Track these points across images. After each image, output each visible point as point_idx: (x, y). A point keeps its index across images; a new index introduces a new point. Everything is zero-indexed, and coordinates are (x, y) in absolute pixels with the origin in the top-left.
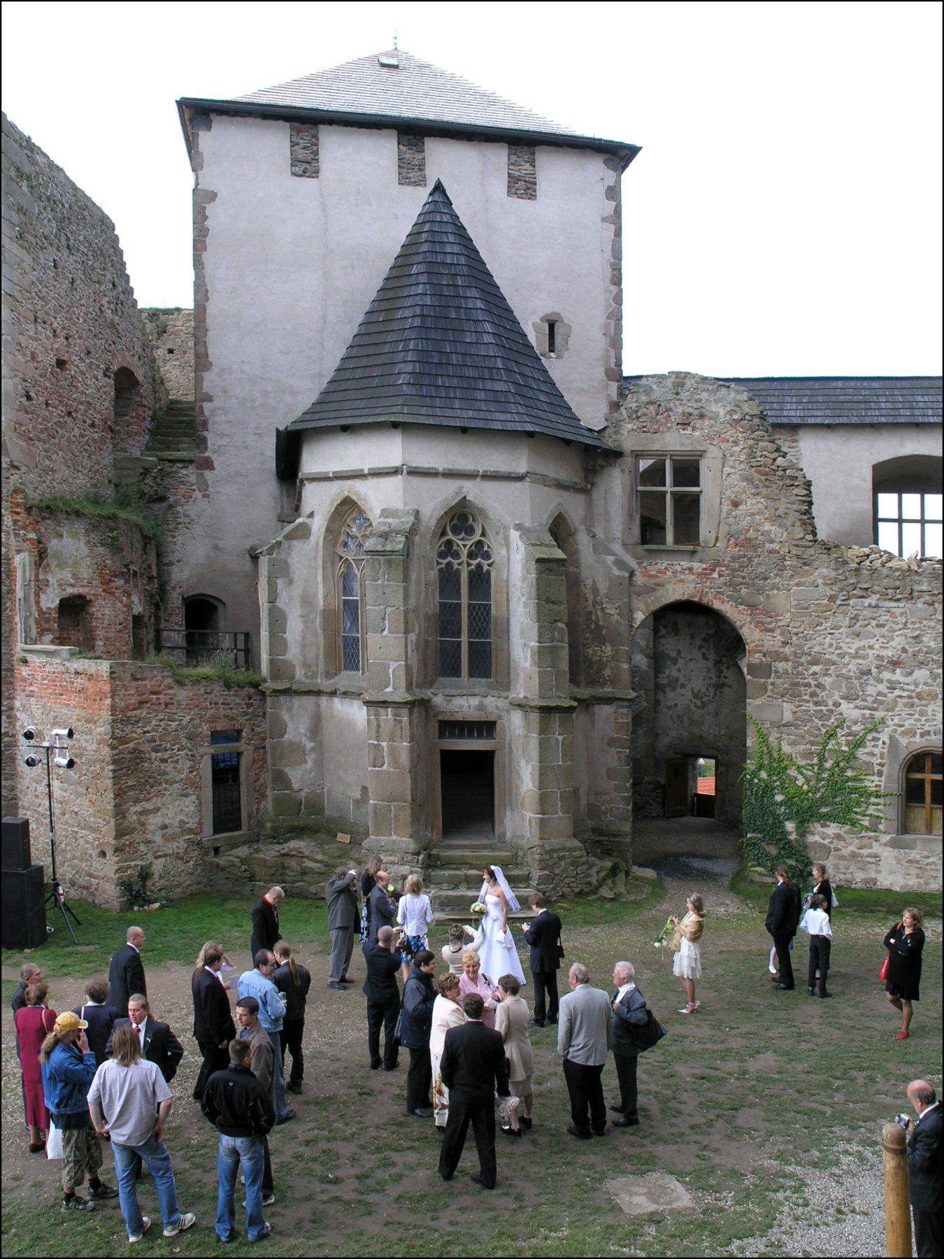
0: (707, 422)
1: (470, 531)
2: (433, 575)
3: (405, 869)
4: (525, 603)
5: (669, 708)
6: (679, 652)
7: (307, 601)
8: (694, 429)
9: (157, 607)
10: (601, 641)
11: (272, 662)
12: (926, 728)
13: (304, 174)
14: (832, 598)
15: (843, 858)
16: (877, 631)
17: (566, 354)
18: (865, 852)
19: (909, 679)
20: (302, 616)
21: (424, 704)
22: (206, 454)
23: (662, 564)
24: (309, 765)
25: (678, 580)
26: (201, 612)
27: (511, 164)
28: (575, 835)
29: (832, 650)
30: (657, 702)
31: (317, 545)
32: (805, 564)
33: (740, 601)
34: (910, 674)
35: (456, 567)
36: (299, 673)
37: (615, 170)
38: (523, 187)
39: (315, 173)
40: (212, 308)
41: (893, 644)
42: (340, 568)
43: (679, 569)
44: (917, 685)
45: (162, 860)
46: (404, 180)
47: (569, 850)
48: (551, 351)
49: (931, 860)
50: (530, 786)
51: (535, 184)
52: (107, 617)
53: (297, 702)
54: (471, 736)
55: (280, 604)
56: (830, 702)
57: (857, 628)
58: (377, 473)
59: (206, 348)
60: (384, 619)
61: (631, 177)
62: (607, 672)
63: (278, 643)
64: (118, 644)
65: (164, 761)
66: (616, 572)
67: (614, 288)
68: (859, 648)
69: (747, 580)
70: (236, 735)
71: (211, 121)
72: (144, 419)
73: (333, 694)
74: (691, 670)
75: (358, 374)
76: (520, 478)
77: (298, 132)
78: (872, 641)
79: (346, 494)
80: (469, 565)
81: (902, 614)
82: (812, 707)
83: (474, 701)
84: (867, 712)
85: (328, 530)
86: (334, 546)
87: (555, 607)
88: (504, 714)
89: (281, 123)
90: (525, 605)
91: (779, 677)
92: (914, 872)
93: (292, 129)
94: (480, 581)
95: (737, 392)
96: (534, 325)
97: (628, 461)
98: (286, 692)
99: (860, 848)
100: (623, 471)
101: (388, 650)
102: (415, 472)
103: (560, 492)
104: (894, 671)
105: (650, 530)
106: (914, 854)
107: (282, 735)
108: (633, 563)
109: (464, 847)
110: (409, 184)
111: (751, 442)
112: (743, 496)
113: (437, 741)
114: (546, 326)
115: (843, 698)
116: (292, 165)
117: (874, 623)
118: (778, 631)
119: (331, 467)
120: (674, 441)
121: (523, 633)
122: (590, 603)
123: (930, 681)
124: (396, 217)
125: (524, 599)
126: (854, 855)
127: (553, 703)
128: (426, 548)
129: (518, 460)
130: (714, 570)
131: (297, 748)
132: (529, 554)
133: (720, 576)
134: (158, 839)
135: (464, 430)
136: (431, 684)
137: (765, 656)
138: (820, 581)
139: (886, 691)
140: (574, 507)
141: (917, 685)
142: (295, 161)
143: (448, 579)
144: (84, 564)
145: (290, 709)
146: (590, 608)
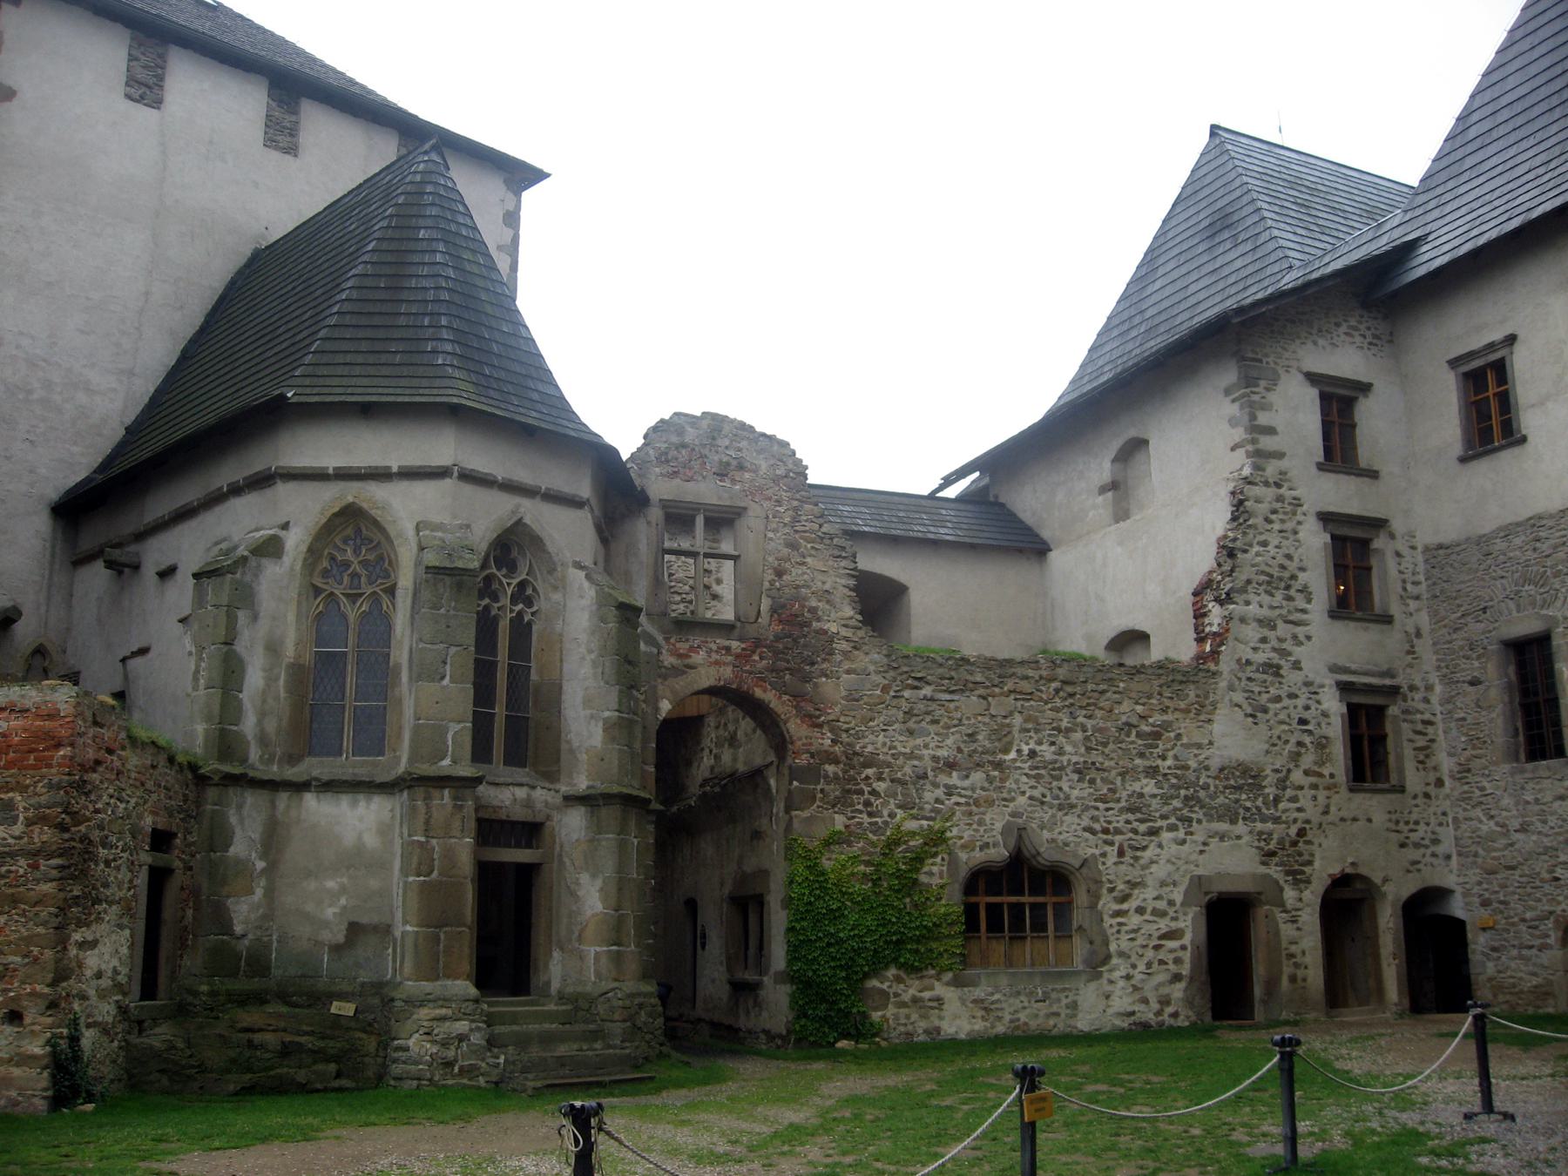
0: (747, 475)
1: (512, 568)
3: (462, 1026)
4: (593, 662)
7: (273, 648)
8: (733, 481)
12: (986, 839)
13: (140, 100)
14: (885, 689)
15: (903, 1005)
16: (932, 728)
18: (927, 995)
19: (966, 783)
20: (265, 670)
24: (259, 892)
29: (885, 750)
31: (292, 569)
32: (855, 648)
33: (782, 689)
34: (967, 777)
36: (254, 754)
39: (157, 103)
41: (949, 742)
42: (318, 604)
43: (714, 647)
44: (973, 790)
49: (996, 997)
50: (599, 907)
55: (239, 647)
56: (885, 813)
57: (911, 724)
60: (445, 663)
69: (792, 665)
77: (140, 45)
78: (928, 739)
79: (350, 499)
81: (957, 708)
82: (866, 819)
83: (521, 793)
84: (925, 823)
86: (311, 575)
88: (556, 816)
89: (119, 27)
90: (594, 664)
91: (828, 783)
92: (980, 1013)
100: (649, 523)
102: (468, 477)
104: (950, 775)
106: (978, 993)
109: (512, 1004)
110: (277, 148)
112: (787, 565)
115: (899, 807)
116: (127, 84)
117: (928, 718)
121: (587, 702)
123: (986, 785)
124: (256, 185)
126: (915, 1000)
131: (243, 867)
137: (812, 756)
138: (872, 668)
139: (944, 797)
141: (973, 790)
142: (131, 81)
145: (240, 807)
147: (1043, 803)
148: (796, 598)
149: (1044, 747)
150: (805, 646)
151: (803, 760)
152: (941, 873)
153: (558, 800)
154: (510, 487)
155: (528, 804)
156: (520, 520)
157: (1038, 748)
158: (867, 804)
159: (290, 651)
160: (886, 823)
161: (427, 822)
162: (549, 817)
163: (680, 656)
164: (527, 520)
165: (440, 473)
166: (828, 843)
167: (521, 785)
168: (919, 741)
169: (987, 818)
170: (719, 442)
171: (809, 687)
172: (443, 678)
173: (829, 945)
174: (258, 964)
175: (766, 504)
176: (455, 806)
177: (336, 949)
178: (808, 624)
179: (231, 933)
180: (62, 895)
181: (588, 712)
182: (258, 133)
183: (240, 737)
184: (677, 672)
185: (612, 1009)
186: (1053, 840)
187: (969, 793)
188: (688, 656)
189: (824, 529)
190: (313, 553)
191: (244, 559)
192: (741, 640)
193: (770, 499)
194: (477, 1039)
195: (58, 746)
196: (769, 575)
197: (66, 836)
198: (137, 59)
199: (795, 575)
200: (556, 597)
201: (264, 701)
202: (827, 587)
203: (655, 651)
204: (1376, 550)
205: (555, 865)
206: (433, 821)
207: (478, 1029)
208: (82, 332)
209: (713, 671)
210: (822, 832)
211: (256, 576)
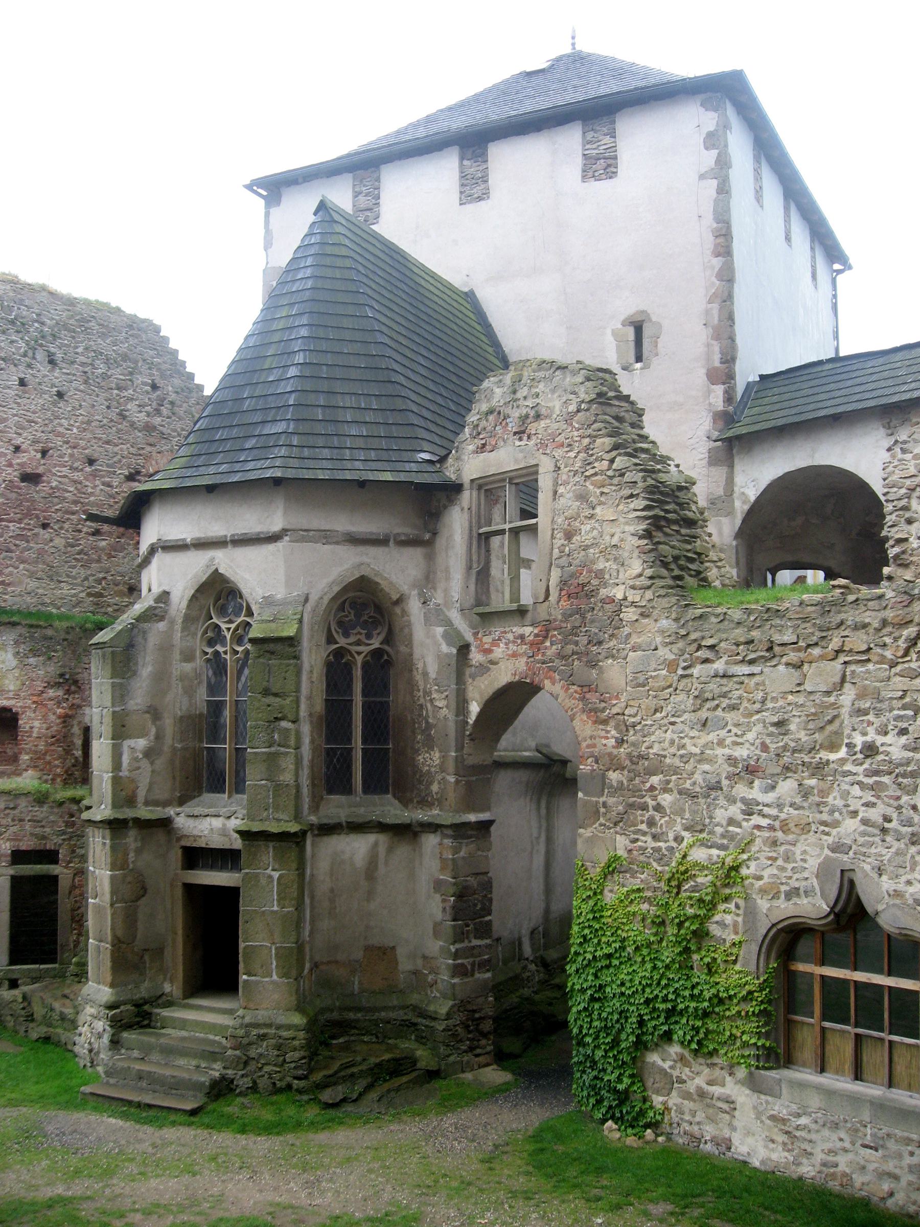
0: (543, 423)
17: (655, 362)
18: (716, 1090)
19: (770, 797)
23: (497, 631)
27: (585, 142)
29: (673, 750)
34: (773, 788)
41: (750, 736)
43: (510, 636)
44: (780, 806)
47: (279, 1027)
48: (639, 359)
51: (615, 158)
52: (35, 730)
56: (671, 836)
64: (48, 758)
67: (717, 262)
68: (705, 746)
76: (273, 538)
78: (723, 733)
82: (651, 844)
83: (217, 823)
87: (278, 700)
93: (354, 179)
96: (615, 333)
99: (710, 1083)
103: (361, 549)
106: (780, 1108)
108: (469, 636)
111: (586, 441)
113: (179, 871)
114: (631, 331)
115: (686, 829)
118: (612, 723)
123: (798, 800)
127: (256, 827)
129: (271, 516)
133: (552, 645)
135: (211, 489)
136: (182, 802)
139: (740, 817)
141: (780, 806)
144: (10, 676)
146: (422, 701)
147: (884, 831)
149: (888, 739)
152: (735, 924)
154: (201, 545)
156: (217, 570)
157: (880, 740)
158: (651, 823)
160: (671, 849)
168: (713, 737)
169: (798, 850)
175: (558, 453)
186: (898, 894)
187: (773, 812)
202: (615, 541)
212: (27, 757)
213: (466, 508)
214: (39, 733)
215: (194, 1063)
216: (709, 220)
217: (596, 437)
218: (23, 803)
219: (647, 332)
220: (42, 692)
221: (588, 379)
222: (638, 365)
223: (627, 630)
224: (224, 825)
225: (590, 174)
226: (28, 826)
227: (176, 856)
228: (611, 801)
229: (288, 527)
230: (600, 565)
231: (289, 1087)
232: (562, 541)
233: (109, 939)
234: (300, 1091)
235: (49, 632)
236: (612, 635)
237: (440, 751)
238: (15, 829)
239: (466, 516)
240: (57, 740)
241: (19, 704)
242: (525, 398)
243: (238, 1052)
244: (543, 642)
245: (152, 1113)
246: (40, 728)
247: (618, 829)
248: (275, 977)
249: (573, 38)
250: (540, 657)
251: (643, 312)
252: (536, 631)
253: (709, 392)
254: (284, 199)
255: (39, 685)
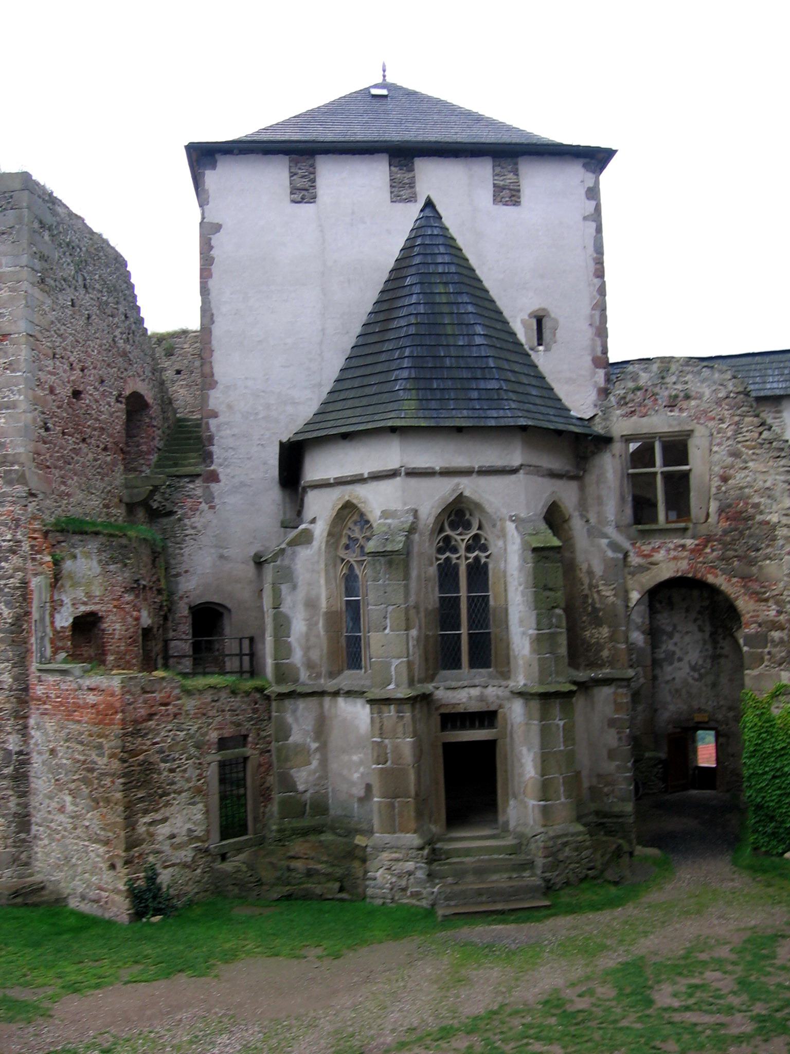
0: (693, 403)
1: (468, 526)
2: (433, 571)
3: (410, 865)
4: (522, 592)
5: (667, 682)
6: (675, 627)
7: (311, 604)
8: (681, 410)
9: (166, 618)
10: (597, 622)
11: (277, 667)
13: (302, 201)
17: (554, 347)
21: (426, 699)
22: (212, 468)
23: (656, 543)
24: (315, 763)
25: (668, 560)
26: (208, 618)
28: (579, 818)
30: (655, 678)
31: (320, 549)
33: (731, 574)
35: (454, 561)
36: (304, 675)
37: (594, 172)
38: (509, 195)
39: (313, 199)
40: (218, 330)
42: (342, 570)
43: (671, 546)
45: (170, 870)
46: (396, 198)
51: (519, 191)
52: (117, 632)
53: (301, 704)
54: (472, 727)
55: (284, 609)
58: (377, 477)
59: (212, 368)
60: (385, 617)
61: (609, 177)
62: (605, 653)
63: (282, 648)
64: (128, 657)
65: (172, 771)
66: (610, 554)
67: (597, 281)
69: (739, 553)
70: (243, 739)
71: (216, 162)
72: (154, 438)
73: (336, 694)
74: (687, 649)
75: (356, 383)
76: (514, 471)
79: (347, 498)
80: (467, 558)
83: (475, 692)
85: (330, 534)
86: (336, 549)
89: (281, 156)
90: (523, 595)
91: (776, 646)
93: (290, 161)
94: (479, 572)
95: (722, 372)
97: (617, 447)
98: (292, 695)
101: (391, 647)
102: (413, 473)
105: (642, 509)
107: (287, 738)
108: (627, 545)
111: (737, 419)
114: (534, 322)
116: (292, 193)
119: (332, 473)
120: (660, 422)
121: (521, 621)
122: (586, 586)
125: (521, 588)
128: (425, 545)
129: (515, 455)
130: (706, 546)
131: (302, 750)
132: (525, 544)
133: (713, 551)
134: (166, 848)
136: (431, 678)
137: (760, 625)
140: (568, 494)
142: (294, 190)
143: (447, 574)
144: (96, 583)
145: (294, 711)
148: (740, 498)
150: (750, 536)
151: (752, 629)
153: (507, 693)
154: (447, 473)
155: (482, 698)
156: (461, 493)
159: (323, 604)
161: (381, 729)
162: (501, 706)
163: (645, 556)
164: (467, 493)
165: (393, 474)
166: (775, 696)
167: (475, 686)
170: (667, 380)
171: (754, 569)
172: (385, 629)
173: (774, 777)
174: (320, 807)
175: (711, 424)
176: (398, 717)
177: (361, 800)
178: (752, 518)
179: (296, 791)
180: (126, 799)
181: (522, 629)
182: (385, 194)
183: (292, 667)
184: (642, 569)
185: (538, 848)
188: (651, 556)
189: (763, 436)
190: (333, 535)
191: (283, 550)
192: (693, 537)
193: (714, 419)
194: (421, 874)
195: (116, 713)
196: (716, 482)
197: (126, 765)
198: (295, 174)
199: (739, 478)
200: (500, 543)
201: (308, 640)
202: (768, 484)
203: (620, 556)
204: (127, 897)
205: (508, 739)
206: (384, 727)
207: (421, 868)
208: (285, 367)
209: (672, 565)
210: (770, 687)
211: (293, 560)
212: (112, 658)
213: (617, 454)
214: (120, 634)
215: (506, 876)
216: (591, 250)
217: (745, 416)
218: (223, 695)
219: (547, 324)
220: (121, 596)
221: (734, 377)
222: (541, 348)
223: (781, 542)
224: (482, 693)
225: (499, 199)
226: (228, 715)
227: (436, 720)
228: (774, 650)
229: (524, 463)
230: (756, 500)
231: (587, 876)
232: (719, 483)
233: (413, 793)
234: (594, 878)
235: (124, 541)
236: (768, 546)
237: (609, 627)
238: (219, 719)
239: (617, 461)
240: (134, 641)
241: (104, 609)
242: (674, 383)
243: (550, 859)
244: (703, 550)
245: (520, 914)
246: (121, 630)
247: (782, 667)
248: (563, 800)
249: (384, 71)
250: (701, 559)
251: (544, 310)
252: (697, 542)
253: (595, 373)
254: (219, 165)
255: (119, 590)
